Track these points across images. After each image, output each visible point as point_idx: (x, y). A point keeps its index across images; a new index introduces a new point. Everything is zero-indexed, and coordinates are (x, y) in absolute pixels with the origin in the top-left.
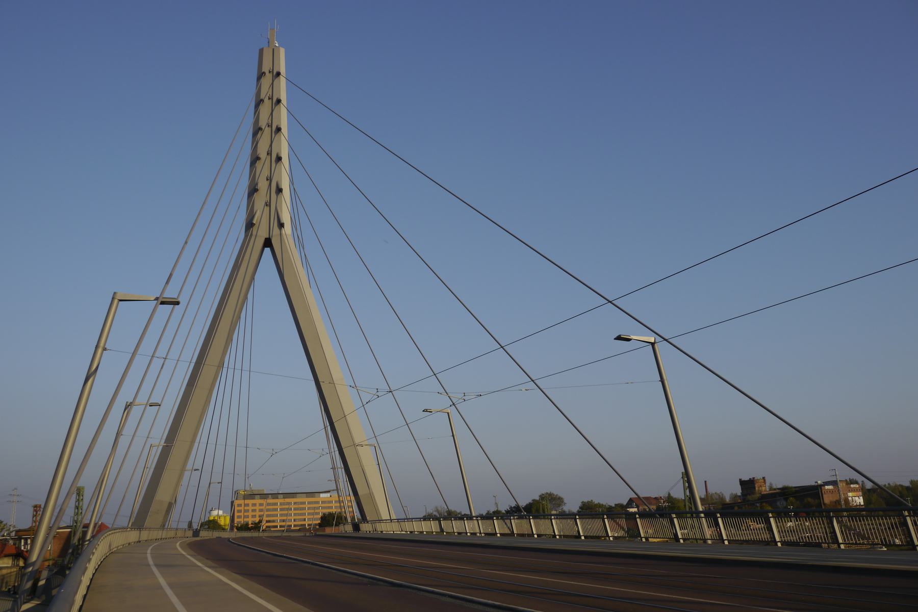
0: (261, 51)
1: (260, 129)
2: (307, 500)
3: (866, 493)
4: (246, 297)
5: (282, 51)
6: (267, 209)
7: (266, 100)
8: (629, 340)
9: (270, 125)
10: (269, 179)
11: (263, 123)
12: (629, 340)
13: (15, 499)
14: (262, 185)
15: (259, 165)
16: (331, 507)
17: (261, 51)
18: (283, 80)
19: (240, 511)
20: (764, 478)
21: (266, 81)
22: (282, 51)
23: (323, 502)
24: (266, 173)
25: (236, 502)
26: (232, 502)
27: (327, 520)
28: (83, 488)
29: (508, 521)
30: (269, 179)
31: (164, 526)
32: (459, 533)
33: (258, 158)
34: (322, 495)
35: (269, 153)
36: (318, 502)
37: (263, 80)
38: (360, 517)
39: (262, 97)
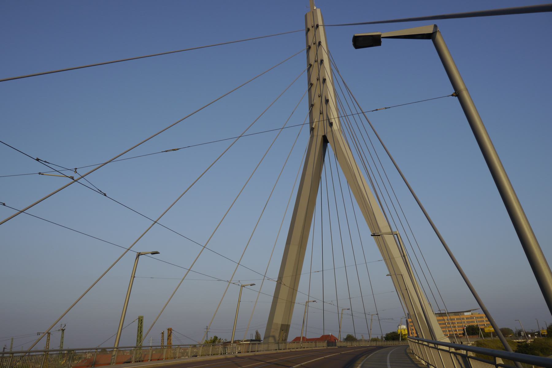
0: (306, 16)
1: (311, 65)
2: (455, 317)
3: (494, 363)
4: (320, 177)
5: (318, 11)
11: (312, 62)
14: (317, 101)
15: (313, 89)
16: (474, 322)
17: (306, 16)
18: (321, 28)
20: (170, 330)
21: (311, 34)
22: (318, 11)
23: (467, 318)
26: (407, 320)
28: (142, 317)
31: (286, 340)
33: (312, 85)
34: (466, 314)
36: (463, 319)
37: (309, 33)
39: (310, 44)
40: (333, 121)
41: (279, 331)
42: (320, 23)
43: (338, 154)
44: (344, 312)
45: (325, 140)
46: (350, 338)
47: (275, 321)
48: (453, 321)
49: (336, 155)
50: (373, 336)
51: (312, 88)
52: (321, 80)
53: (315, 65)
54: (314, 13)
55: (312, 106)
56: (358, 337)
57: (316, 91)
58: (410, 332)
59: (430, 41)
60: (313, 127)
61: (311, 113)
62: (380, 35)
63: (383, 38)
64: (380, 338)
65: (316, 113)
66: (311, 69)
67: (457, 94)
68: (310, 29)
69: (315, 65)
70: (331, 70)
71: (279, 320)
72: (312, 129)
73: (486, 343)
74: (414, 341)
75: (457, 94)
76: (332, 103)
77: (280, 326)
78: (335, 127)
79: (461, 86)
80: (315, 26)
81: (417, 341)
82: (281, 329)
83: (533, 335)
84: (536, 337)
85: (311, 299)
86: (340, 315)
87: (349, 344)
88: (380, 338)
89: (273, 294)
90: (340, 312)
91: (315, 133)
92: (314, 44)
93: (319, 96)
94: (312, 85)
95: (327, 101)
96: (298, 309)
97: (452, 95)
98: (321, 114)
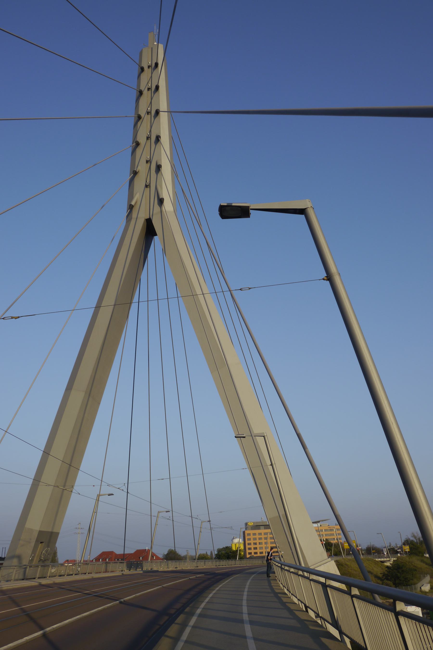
11: (142, 112)
14: (142, 168)
15: (139, 151)
19: (249, 544)
25: (247, 532)
33: (138, 144)
39: (142, 88)
40: (165, 195)
41: (33, 544)
44: (161, 514)
45: (150, 231)
46: (172, 556)
47: (28, 525)
48: (321, 533)
50: (201, 552)
51: (137, 149)
52: (153, 138)
56: (182, 552)
57: (143, 154)
58: (247, 547)
59: (303, 216)
60: (133, 203)
62: (248, 207)
63: (251, 209)
64: (209, 553)
65: (140, 183)
66: (139, 123)
69: (146, 119)
70: (172, 138)
71: (35, 524)
72: (131, 207)
73: (348, 563)
74: (277, 564)
75: (329, 278)
77: (36, 535)
78: (168, 206)
79: (333, 269)
80: (153, 65)
81: (280, 565)
82: (37, 541)
83: (393, 551)
84: (399, 555)
85: (106, 490)
86: (154, 519)
87: (172, 566)
88: (209, 553)
90: (154, 513)
91: (134, 215)
92: (149, 89)
93: (147, 162)
94: (138, 144)
95: (159, 168)
96: (78, 507)
97: (323, 279)
98: (146, 186)
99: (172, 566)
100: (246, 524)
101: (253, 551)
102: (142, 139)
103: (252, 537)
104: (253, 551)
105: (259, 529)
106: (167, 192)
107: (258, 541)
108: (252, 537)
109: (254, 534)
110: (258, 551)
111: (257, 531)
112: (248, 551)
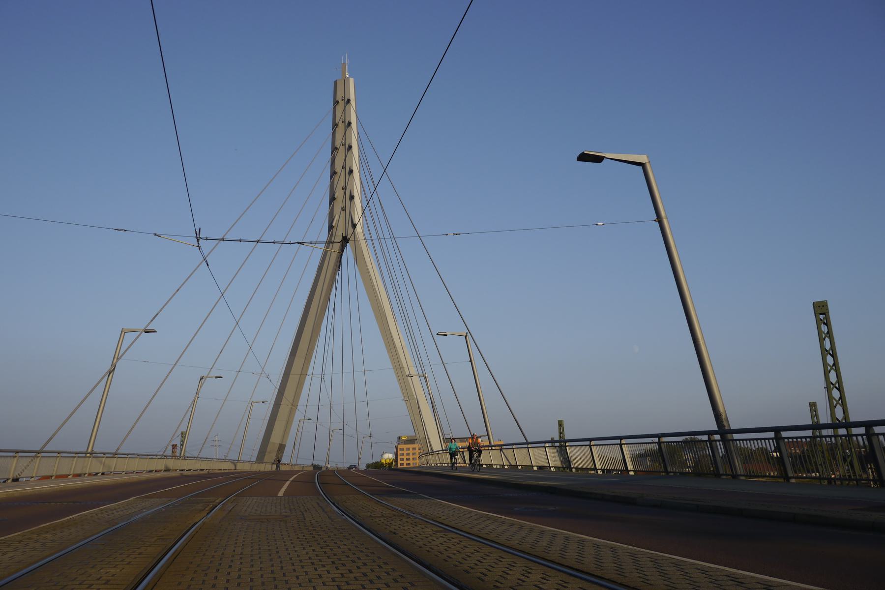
0: (336, 82)
1: (336, 148)
6: (343, 213)
7: (340, 124)
8: (598, 159)
9: (344, 145)
10: (345, 189)
12: (598, 159)
13: (217, 443)
14: (339, 194)
15: (336, 178)
17: (336, 82)
19: (402, 454)
22: (352, 81)
24: (341, 184)
25: (399, 447)
27: (351, 467)
29: (839, 413)
30: (345, 189)
32: (540, 468)
35: (344, 167)
38: (863, 429)
40: (356, 221)
42: (352, 98)
43: (358, 258)
45: (345, 240)
49: (356, 258)
53: (342, 149)
54: (345, 82)
55: (333, 199)
58: (399, 457)
61: (334, 134)
67: (659, 220)
68: (340, 102)
69: (342, 149)
71: (183, 428)
75: (659, 220)
76: (357, 200)
78: (359, 229)
89: (388, 364)
99: (167, 474)
100: (399, 438)
101: (405, 462)
102: (338, 169)
103: (405, 452)
104: (405, 462)
105: (414, 443)
106: (357, 217)
107: (411, 457)
108: (405, 452)
109: (408, 449)
110: (411, 462)
111: (411, 446)
112: (399, 462)
